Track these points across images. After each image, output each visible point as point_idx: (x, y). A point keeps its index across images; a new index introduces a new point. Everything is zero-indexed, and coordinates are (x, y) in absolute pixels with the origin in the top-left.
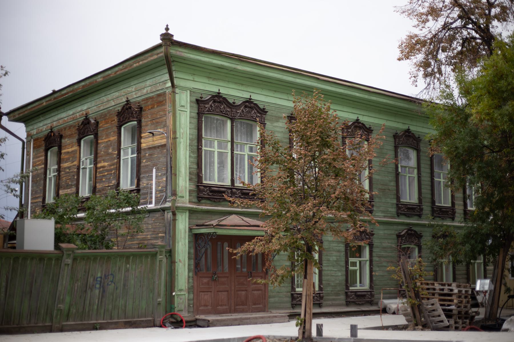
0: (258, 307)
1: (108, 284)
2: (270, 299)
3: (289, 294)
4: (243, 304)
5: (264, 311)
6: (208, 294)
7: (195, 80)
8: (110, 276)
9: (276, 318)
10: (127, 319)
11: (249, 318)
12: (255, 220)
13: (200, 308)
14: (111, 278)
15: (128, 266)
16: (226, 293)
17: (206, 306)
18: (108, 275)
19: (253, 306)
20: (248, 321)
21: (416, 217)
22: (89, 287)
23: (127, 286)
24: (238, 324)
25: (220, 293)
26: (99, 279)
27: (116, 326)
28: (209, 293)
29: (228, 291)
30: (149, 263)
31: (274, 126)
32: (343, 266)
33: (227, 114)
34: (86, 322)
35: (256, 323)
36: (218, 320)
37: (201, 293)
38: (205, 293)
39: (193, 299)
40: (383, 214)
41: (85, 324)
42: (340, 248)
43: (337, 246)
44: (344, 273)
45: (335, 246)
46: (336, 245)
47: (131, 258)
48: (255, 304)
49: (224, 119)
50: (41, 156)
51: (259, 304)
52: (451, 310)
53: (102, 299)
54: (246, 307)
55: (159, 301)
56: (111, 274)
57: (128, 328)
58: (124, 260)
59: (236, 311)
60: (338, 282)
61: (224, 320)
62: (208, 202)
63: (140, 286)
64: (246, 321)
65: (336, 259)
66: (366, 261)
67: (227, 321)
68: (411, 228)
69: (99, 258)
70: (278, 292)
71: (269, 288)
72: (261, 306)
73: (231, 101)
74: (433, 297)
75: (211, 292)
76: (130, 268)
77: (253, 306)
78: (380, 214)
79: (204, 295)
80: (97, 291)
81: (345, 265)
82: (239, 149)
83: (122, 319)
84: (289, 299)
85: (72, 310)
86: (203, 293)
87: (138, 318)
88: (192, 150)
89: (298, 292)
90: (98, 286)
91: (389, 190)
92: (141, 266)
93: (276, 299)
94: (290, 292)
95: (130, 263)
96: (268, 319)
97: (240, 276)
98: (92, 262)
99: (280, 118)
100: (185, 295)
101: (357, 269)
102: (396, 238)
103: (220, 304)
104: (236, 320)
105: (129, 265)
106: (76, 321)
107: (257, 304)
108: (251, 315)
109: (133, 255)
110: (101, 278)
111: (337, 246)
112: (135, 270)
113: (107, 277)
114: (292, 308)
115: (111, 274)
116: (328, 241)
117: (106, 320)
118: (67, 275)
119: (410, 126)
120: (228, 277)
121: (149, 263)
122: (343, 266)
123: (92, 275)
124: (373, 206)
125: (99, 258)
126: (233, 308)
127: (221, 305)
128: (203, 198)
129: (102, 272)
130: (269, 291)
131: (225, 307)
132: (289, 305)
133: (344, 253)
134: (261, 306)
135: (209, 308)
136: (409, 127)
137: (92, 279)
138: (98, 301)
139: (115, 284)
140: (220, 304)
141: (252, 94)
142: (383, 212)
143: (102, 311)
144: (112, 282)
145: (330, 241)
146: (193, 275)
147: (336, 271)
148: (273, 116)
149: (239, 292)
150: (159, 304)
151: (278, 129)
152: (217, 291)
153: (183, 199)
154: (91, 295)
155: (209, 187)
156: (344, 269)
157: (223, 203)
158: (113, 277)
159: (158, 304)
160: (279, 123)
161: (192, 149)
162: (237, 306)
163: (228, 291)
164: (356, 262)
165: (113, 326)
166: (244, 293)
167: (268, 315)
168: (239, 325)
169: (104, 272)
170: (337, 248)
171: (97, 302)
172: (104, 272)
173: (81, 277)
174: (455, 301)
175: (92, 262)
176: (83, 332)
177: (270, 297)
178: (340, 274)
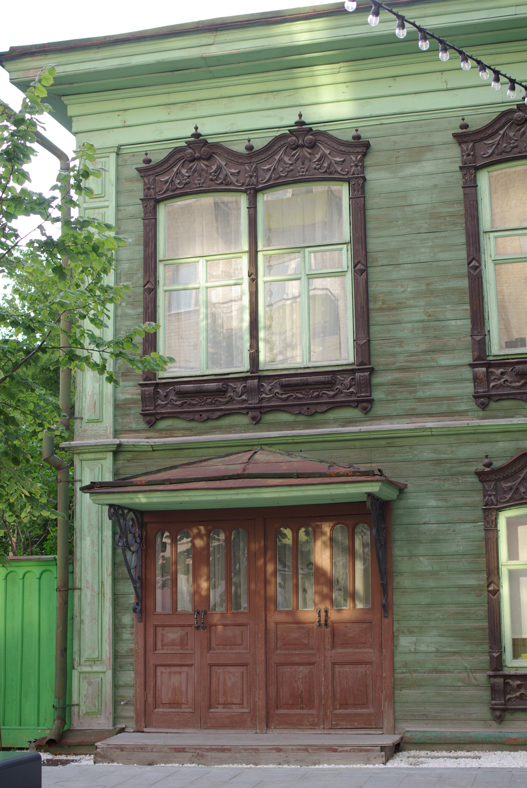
6: (180, 673)
7: (128, 123)
17: (174, 704)
28: (185, 669)
29: (246, 665)
31: (403, 178)
33: (231, 184)
38: (174, 669)
50: (83, 352)
73: (241, 148)
75: (191, 665)
88: (131, 300)
99: (429, 148)
100: (104, 672)
114: (494, 723)
119: (304, 110)
127: (225, 705)
131: (236, 710)
135: (185, 709)
136: (300, 116)
140: (221, 701)
141: (198, 122)
148: (398, 150)
151: (418, 183)
153: (96, 426)
160: (424, 164)
161: (129, 297)
166: (303, 670)
176: (221, 731)
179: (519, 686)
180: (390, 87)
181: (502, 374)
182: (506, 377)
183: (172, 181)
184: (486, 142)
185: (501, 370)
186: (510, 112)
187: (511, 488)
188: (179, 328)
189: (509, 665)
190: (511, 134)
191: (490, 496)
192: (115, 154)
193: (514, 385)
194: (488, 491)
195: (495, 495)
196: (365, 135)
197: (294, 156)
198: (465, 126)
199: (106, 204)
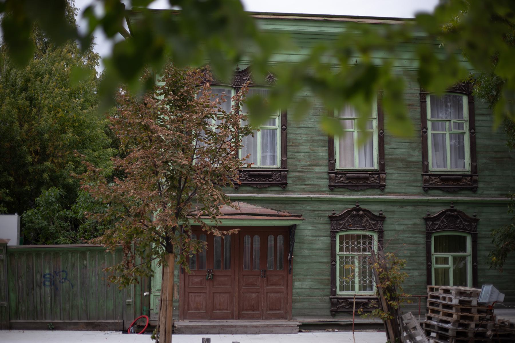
0: (276, 313)
1: (60, 282)
2: (296, 304)
3: (327, 299)
4: (253, 309)
5: (285, 318)
8: (61, 273)
9: (278, 328)
10: (89, 320)
11: (235, 326)
12: (260, 207)
13: (189, 312)
14: (63, 275)
15: (85, 262)
16: (227, 295)
18: (60, 272)
19: (268, 312)
20: (233, 329)
21: (378, 191)
22: (37, 285)
23: (87, 284)
24: (217, 332)
25: (218, 295)
26: (48, 276)
27: (76, 327)
29: (230, 293)
30: (114, 258)
32: (422, 264)
34: (38, 321)
35: (245, 333)
36: (187, 327)
37: (190, 294)
38: (197, 294)
39: (179, 301)
40: (499, 192)
41: (37, 323)
42: (418, 239)
43: (411, 237)
44: (425, 272)
45: (408, 237)
46: (410, 236)
47: (88, 253)
48: (271, 310)
49: (230, 89)
51: (279, 310)
52: (446, 330)
53: (55, 297)
54: (257, 312)
55: (129, 302)
56: (63, 271)
57: (90, 330)
58: (78, 256)
59: (240, 317)
60: (413, 284)
61: (197, 327)
62: (249, 188)
63: (104, 285)
64: (230, 329)
65: (409, 254)
66: (468, 255)
67: (201, 328)
68: (452, 207)
69: (43, 254)
70: (309, 296)
71: (294, 291)
72: (282, 312)
74: (132, 305)
75: (205, 293)
76: (88, 265)
77: (268, 312)
78: (494, 192)
79: (195, 296)
80: (48, 289)
81: (425, 261)
82: (440, 128)
83: (84, 320)
84: (328, 305)
85: (20, 307)
86: (193, 295)
87: (104, 319)
89: (340, 297)
90: (47, 283)
91: (510, 158)
92: (104, 263)
93: (306, 304)
94: (328, 296)
95: (88, 260)
96: (266, 328)
97: (248, 275)
98: (34, 258)
101: (450, 267)
102: (329, 222)
103: (218, 307)
104: (214, 327)
105: (87, 261)
106: (28, 319)
107: (275, 310)
108: (251, 322)
109: (90, 250)
110: (50, 275)
111: (411, 237)
112: (95, 267)
113: (58, 274)
115: (63, 271)
116: (395, 230)
117: (63, 320)
118: (3, 271)
120: (230, 276)
121: (114, 258)
122: (422, 264)
123: (38, 272)
124: (476, 182)
125: (43, 254)
126: (236, 313)
127: (220, 309)
128: (429, 188)
129: (50, 268)
130: (294, 293)
131: (225, 312)
132: (327, 312)
133: (425, 246)
134: (282, 312)
135: (202, 311)
137: (38, 276)
138: (51, 299)
139: (69, 281)
142: (497, 189)
143: (58, 310)
144: (65, 279)
145: (399, 231)
146: (179, 273)
147: (409, 269)
149: (247, 295)
150: (129, 305)
152: (214, 293)
154: (40, 293)
155: (343, 173)
156: (424, 267)
157: (269, 189)
158: (67, 274)
159: (127, 305)
162: (243, 310)
163: (230, 293)
164: (447, 258)
165: (72, 327)
166: (254, 295)
167: (286, 323)
168: (219, 334)
169: (52, 269)
170: (412, 240)
171: (49, 301)
172: (52, 269)
173: (24, 274)
174: (455, 316)
175: (34, 258)
176: (27, 332)
177: (295, 301)
178: (416, 273)
181: (341, 177)
189: (338, 294)
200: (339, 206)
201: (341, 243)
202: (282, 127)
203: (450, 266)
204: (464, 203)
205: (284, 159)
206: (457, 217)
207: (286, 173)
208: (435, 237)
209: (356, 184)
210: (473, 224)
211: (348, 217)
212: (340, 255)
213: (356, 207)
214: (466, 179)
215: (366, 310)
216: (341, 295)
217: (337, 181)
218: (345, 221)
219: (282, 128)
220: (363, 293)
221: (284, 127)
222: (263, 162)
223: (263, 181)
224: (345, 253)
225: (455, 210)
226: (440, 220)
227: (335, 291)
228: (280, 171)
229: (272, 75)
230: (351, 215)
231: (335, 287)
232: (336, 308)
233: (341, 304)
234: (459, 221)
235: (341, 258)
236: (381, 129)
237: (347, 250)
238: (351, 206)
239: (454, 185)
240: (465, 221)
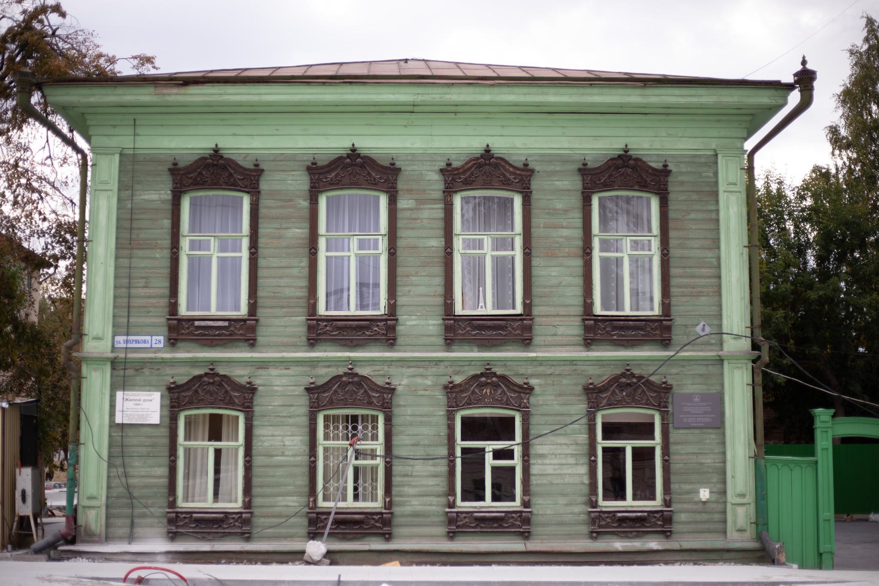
101: (379, 464)
179: (465, 517)
180: (277, 130)
181: (326, 326)
182: (328, 328)
183: (196, 178)
184: (189, 176)
185: (325, 323)
186: (477, 159)
187: (606, 397)
188: (130, 278)
189: (600, 505)
190: (204, 173)
191: (593, 402)
192: (118, 155)
193: (196, 332)
194: (591, 399)
195: (317, 402)
196: (398, 164)
197: (481, 171)
198: (175, 164)
199: (111, 188)
200: (182, 370)
201: (326, 427)
202: (524, 251)
203: (379, 463)
204: (371, 362)
205: (528, 302)
206: (359, 385)
207: (394, 322)
208: (186, 417)
209: (353, 336)
210: (386, 396)
211: (614, 386)
212: (325, 446)
213: (625, 371)
214: (378, 326)
215: (222, 531)
216: (606, 507)
217: (319, 332)
218: (610, 393)
219: (524, 253)
220: (361, 504)
221: (392, 251)
222: (636, 306)
223: (633, 336)
224: (331, 442)
225: (356, 375)
226: (609, 390)
227: (597, 501)
228: (386, 320)
229: (232, 171)
230: (618, 385)
231: (597, 495)
232: (455, 527)
233: (462, 521)
234: (499, 392)
235: (326, 450)
236: (253, 247)
237: (336, 438)
238: (341, 371)
239: (358, 336)
240: (373, 390)
